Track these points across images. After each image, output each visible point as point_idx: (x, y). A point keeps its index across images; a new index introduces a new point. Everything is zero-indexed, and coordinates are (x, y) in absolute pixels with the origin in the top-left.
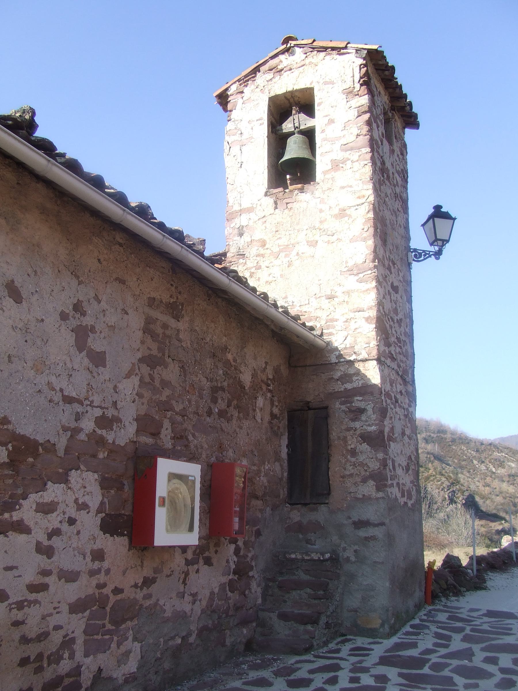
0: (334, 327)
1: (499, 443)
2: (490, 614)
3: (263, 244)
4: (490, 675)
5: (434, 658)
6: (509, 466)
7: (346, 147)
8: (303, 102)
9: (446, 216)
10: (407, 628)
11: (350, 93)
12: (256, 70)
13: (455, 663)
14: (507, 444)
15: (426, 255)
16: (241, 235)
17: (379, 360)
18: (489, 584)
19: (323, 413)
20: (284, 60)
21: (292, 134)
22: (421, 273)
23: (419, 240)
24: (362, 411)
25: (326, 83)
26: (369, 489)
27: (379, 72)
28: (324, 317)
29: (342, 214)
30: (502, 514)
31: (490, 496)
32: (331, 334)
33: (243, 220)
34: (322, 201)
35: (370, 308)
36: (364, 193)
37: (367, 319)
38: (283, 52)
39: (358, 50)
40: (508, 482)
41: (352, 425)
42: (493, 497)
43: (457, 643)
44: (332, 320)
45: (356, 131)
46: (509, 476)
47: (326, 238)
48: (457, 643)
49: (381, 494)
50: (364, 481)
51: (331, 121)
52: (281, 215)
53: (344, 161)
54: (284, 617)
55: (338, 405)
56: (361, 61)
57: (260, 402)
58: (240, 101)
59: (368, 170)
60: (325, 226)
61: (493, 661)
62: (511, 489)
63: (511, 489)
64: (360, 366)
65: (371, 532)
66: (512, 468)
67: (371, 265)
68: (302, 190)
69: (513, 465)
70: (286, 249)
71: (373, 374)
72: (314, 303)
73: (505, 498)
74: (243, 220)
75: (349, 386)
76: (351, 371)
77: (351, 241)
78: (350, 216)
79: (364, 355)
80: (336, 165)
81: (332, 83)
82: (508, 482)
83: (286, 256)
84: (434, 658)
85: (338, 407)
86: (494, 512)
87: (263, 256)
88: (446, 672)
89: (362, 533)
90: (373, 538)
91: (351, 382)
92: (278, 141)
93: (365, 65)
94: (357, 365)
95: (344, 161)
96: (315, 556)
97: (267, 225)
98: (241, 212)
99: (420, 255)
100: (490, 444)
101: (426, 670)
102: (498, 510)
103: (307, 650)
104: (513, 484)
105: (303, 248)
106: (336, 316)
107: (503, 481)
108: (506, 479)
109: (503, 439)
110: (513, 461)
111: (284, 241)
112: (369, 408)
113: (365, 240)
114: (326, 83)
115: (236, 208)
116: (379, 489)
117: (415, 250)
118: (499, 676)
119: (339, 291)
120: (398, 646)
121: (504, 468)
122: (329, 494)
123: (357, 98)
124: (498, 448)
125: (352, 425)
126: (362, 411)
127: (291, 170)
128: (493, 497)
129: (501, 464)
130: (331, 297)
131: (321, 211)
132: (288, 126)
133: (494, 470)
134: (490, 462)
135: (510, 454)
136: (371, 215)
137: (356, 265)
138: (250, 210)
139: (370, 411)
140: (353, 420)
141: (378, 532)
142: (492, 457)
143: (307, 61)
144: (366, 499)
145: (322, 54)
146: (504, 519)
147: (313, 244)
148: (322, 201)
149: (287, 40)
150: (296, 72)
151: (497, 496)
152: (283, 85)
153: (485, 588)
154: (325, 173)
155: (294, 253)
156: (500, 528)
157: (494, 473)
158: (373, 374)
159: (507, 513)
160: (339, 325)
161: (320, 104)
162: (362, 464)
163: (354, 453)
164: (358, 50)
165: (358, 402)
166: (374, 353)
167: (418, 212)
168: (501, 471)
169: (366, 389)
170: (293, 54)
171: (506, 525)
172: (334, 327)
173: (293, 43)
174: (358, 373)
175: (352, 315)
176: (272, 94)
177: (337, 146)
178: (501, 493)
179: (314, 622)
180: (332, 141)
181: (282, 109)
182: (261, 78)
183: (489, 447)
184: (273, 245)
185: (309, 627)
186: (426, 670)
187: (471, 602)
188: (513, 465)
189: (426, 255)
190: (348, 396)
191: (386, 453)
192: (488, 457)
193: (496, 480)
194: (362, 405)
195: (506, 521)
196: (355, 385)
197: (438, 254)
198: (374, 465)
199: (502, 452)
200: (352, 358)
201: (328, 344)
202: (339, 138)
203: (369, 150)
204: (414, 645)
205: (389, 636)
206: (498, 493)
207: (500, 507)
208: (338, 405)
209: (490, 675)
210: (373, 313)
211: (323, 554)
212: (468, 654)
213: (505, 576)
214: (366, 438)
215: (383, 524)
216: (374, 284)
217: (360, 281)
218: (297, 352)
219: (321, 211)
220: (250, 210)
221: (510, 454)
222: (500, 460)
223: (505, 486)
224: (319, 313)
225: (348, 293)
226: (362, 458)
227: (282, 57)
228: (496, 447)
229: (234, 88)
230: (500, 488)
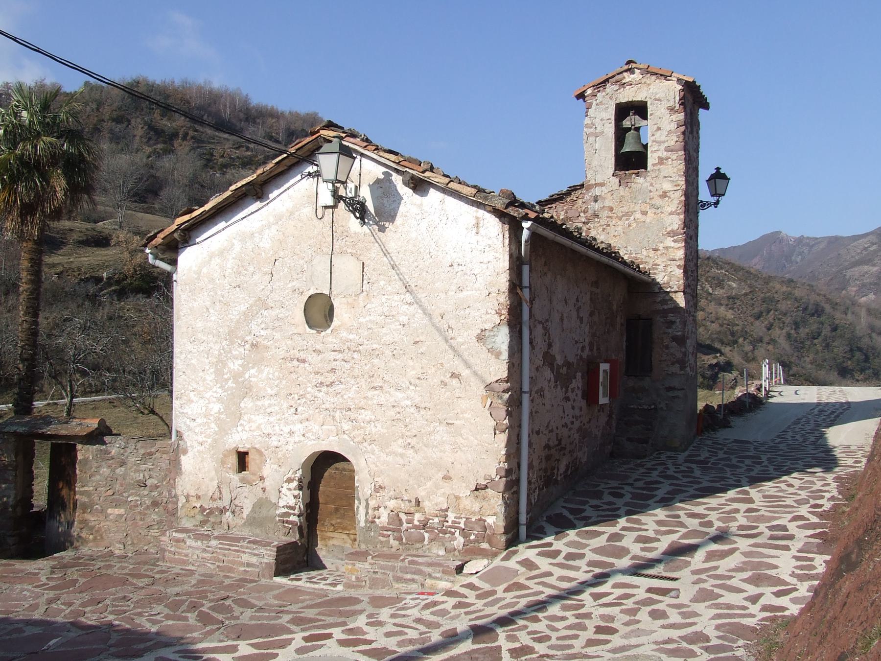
0: (657, 269)
1: (719, 257)
2: (736, 441)
3: (611, 209)
4: (741, 467)
5: (712, 461)
6: (729, 286)
7: (668, 149)
8: (640, 109)
9: (724, 177)
10: (691, 448)
11: (672, 109)
12: (607, 80)
13: (723, 462)
14: (728, 258)
15: (709, 204)
16: (596, 201)
17: (684, 292)
18: (732, 424)
19: (649, 322)
20: (628, 77)
21: (629, 129)
22: (704, 216)
23: (704, 194)
24: (673, 323)
25: (656, 100)
26: (676, 369)
27: (693, 99)
28: (651, 263)
29: (664, 195)
30: (717, 345)
31: (704, 322)
32: (655, 274)
33: (597, 191)
34: (651, 185)
35: (680, 259)
36: (679, 182)
37: (678, 266)
38: (626, 71)
39: (679, 80)
40: (727, 305)
41: (667, 331)
42: (708, 323)
43: (721, 455)
44: (656, 265)
45: (675, 139)
46: (729, 298)
47: (654, 210)
48: (721, 455)
49: (682, 372)
50: (673, 364)
51: (659, 129)
52: (622, 191)
53: (667, 159)
54: (630, 440)
55: (658, 318)
56: (680, 87)
57: (618, 318)
58: (595, 103)
59: (682, 167)
60: (653, 202)
61: (743, 462)
62: (730, 315)
63: (730, 315)
64: (673, 295)
65: (676, 393)
66: (733, 289)
67: (682, 231)
68: (637, 175)
69: (734, 285)
70: (627, 215)
71: (680, 300)
72: (645, 252)
73: (721, 325)
74: (597, 191)
75: (666, 307)
76: (667, 298)
77: (670, 214)
78: (669, 198)
79: (675, 289)
80: (661, 161)
81: (660, 100)
82: (727, 305)
83: (627, 220)
84: (712, 461)
85: (659, 319)
86: (708, 342)
87: (611, 217)
88: (720, 466)
89: (671, 394)
90: (677, 397)
91: (667, 304)
92: (621, 134)
93: (683, 90)
94: (671, 294)
95: (667, 159)
96: (646, 407)
97: (614, 196)
98: (596, 185)
99: (705, 205)
100: (708, 258)
101: (709, 465)
102: (713, 340)
103: (645, 457)
104: (732, 308)
105: (638, 215)
106: (658, 262)
107: (721, 304)
108: (724, 302)
109: (722, 250)
110: (734, 280)
111: (625, 209)
112: (678, 321)
113: (678, 214)
114: (656, 100)
115: (592, 182)
116: (681, 369)
117: (701, 202)
118: (746, 468)
119: (661, 246)
120: (690, 456)
121: (723, 288)
122: (651, 371)
123: (677, 115)
124: (717, 264)
125: (667, 331)
126: (673, 323)
127: (631, 161)
128: (708, 323)
129: (720, 284)
130: (655, 250)
131: (651, 191)
132: (626, 123)
133: (710, 290)
134: (706, 281)
135: (731, 271)
136: (683, 198)
137: (673, 231)
138: (602, 185)
139: (678, 324)
140: (667, 328)
141: (680, 394)
142: (709, 274)
143: (643, 81)
144: (673, 375)
145: (654, 77)
146: (719, 351)
147: (645, 213)
148: (651, 185)
149: (629, 62)
150: (636, 88)
151: (713, 322)
152: (627, 95)
153: (731, 427)
154: (654, 165)
155: (632, 218)
156: (714, 361)
157: (711, 294)
158: (680, 300)
159: (722, 343)
160: (661, 267)
161: (651, 115)
162: (672, 354)
163: (667, 347)
164: (679, 80)
165: (671, 317)
166: (682, 288)
167: (705, 172)
168: (719, 292)
169: (676, 308)
170: (633, 73)
171: (722, 359)
172: (657, 269)
173: (634, 65)
174: (672, 299)
175: (669, 263)
176: (618, 102)
177: (662, 147)
178: (717, 319)
179: (647, 442)
180: (660, 143)
181: (623, 110)
182: (610, 88)
183: (706, 262)
184: (618, 211)
185: (645, 445)
186: (709, 465)
187: (723, 435)
188: (734, 285)
189: (709, 204)
190: (665, 312)
191: (685, 347)
192: (704, 275)
193: (713, 303)
194: (673, 319)
195: (722, 354)
196: (669, 306)
197: (716, 204)
198: (679, 355)
199: (722, 268)
200: (669, 290)
201: (654, 279)
202: (664, 142)
203: (683, 153)
204: (699, 455)
205: (684, 451)
206: (713, 319)
207: (715, 336)
208: (658, 318)
209: (741, 467)
210: (682, 263)
211: (650, 406)
212: (729, 459)
213: (741, 419)
214: (675, 339)
215: (683, 389)
216: (683, 244)
217: (674, 241)
218: (635, 284)
219: (651, 191)
220: (602, 185)
221: (731, 271)
222: (718, 279)
223: (722, 310)
224: (648, 260)
225: (667, 248)
226: (672, 351)
227: (625, 74)
228: (715, 262)
229: (589, 92)
230: (717, 313)
